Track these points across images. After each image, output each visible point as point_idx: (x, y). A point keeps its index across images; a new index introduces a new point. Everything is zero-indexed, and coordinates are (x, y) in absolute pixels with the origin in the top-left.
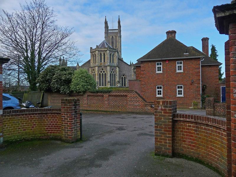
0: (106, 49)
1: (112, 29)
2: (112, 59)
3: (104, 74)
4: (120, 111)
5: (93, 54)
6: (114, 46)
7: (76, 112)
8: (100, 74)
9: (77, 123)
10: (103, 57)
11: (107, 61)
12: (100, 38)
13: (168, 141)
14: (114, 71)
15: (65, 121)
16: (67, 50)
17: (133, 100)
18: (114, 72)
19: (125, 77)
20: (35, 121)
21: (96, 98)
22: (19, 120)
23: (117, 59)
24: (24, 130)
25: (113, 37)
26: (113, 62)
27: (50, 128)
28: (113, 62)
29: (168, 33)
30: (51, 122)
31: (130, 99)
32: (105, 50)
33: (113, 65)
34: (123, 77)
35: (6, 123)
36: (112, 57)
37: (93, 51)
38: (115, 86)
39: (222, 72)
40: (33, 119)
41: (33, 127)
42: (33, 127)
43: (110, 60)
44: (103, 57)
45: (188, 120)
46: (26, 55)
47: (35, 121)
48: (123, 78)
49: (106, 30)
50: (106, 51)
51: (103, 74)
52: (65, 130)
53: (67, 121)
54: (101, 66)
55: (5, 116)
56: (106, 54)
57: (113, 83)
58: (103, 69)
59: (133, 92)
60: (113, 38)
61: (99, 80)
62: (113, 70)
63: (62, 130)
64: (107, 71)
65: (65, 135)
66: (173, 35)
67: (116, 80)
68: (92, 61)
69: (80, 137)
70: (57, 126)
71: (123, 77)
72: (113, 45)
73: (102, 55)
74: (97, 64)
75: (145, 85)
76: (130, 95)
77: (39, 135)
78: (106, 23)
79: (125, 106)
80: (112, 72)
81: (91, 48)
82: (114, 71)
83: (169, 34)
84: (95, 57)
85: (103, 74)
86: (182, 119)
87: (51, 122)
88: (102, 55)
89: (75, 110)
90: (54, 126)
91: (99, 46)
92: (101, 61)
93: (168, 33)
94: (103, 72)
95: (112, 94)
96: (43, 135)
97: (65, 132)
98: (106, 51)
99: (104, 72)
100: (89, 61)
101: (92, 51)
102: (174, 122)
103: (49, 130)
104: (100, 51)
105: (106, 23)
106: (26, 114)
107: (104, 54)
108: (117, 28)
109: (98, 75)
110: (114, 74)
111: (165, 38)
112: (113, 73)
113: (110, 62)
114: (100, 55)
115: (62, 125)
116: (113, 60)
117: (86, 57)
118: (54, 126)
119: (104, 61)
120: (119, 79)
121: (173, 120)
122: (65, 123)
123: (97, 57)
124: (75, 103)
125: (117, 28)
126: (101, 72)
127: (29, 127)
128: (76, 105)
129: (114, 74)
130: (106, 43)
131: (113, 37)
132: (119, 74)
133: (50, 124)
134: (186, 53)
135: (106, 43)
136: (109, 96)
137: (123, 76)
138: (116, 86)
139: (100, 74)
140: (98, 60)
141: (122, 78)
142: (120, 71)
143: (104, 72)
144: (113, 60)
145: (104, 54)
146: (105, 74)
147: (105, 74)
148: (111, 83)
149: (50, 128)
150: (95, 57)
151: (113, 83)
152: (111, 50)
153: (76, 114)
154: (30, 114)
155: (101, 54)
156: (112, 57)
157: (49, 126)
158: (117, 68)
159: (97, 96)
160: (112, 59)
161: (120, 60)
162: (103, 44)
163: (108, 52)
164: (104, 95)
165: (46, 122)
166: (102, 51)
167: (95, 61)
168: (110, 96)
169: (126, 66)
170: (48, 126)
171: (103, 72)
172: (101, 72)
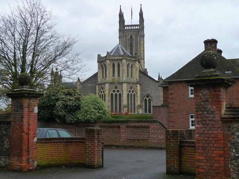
0: (121, 58)
1: (130, 24)
2: (130, 72)
3: (118, 94)
4: (141, 145)
5: (102, 64)
6: (134, 52)
7: (98, 140)
8: (112, 94)
9: (99, 151)
10: (116, 69)
11: (123, 76)
12: (111, 40)
13: (176, 162)
14: (133, 90)
15: (89, 149)
16: (69, 63)
17: (156, 132)
18: (133, 91)
19: (149, 99)
20: (61, 148)
21: (111, 130)
22: (48, 147)
23: (138, 72)
24: (52, 157)
25: (131, 37)
26: (132, 76)
27: (74, 156)
28: (132, 76)
29: (207, 42)
30: (76, 150)
31: (152, 131)
32: (119, 60)
33: (132, 81)
34: (148, 99)
35: (39, 150)
36: (130, 69)
37: (101, 60)
38: (134, 112)
39: (56, 136)
40: (59, 147)
41: (59, 154)
42: (59, 154)
43: (128, 73)
44: (116, 69)
45: (190, 145)
46: (14, 71)
47: (61, 148)
48: (147, 100)
49: (122, 26)
50: (122, 60)
51: (116, 94)
52: (89, 157)
53: (91, 149)
54: (114, 83)
55: (38, 143)
56: (121, 65)
57: (131, 108)
58: (116, 88)
59: (157, 123)
60: (132, 37)
61: (110, 104)
62: (131, 88)
63: (86, 157)
64: (122, 90)
65: (89, 161)
66: (213, 46)
67: (136, 104)
68: (100, 76)
69: (101, 164)
70: (81, 154)
71: (148, 99)
72: (131, 53)
73: (116, 65)
74: (107, 79)
75: (174, 114)
76: (152, 126)
77: (65, 162)
78: (121, 16)
79: (146, 140)
80: (130, 91)
81: (99, 55)
82: (133, 90)
83: (207, 44)
84: (104, 70)
85: (116, 94)
86: (186, 144)
87: (76, 150)
88: (116, 65)
89: (98, 138)
90: (78, 154)
91: (110, 52)
92: (114, 75)
93: (207, 42)
94: (116, 92)
95: (131, 124)
96: (67, 162)
97: (89, 159)
98: (122, 60)
99: (118, 91)
100: (96, 75)
101: (101, 61)
102: (181, 147)
103: (73, 158)
104: (113, 60)
105: (121, 16)
106: (54, 142)
107: (119, 65)
108: (138, 23)
109: (109, 96)
110: (133, 94)
111: (201, 49)
112: (131, 92)
113: (128, 76)
114: (112, 66)
115: (86, 153)
116: (132, 73)
117: (89, 69)
118: (78, 154)
119: (119, 75)
120: (141, 101)
121: (180, 145)
122: (89, 151)
123: (107, 68)
124: (98, 132)
125: (138, 23)
126: (114, 91)
127: (56, 154)
128: (99, 134)
129: (133, 94)
130: (121, 48)
131: (131, 37)
132: (141, 94)
133: (74, 152)
134: (228, 71)
135: (121, 48)
136: (127, 127)
137: (147, 97)
138: (136, 112)
139: (112, 94)
140: (109, 74)
141: (146, 100)
142: (142, 90)
143: (118, 91)
144: (132, 73)
145: (119, 65)
146: (120, 94)
147: (120, 94)
148: (128, 107)
149: (74, 156)
150: (104, 70)
151: (131, 108)
152: (129, 58)
153: (99, 142)
154: (57, 142)
155: (114, 65)
156: (130, 69)
157: (73, 154)
158: (138, 86)
159: (111, 127)
160: (130, 72)
161: (144, 73)
162: (117, 50)
163: (124, 61)
164: (121, 126)
165: (70, 150)
166: (115, 60)
167: (104, 74)
168: (128, 127)
169: (151, 81)
170: (73, 154)
171: (116, 92)
172: (114, 91)
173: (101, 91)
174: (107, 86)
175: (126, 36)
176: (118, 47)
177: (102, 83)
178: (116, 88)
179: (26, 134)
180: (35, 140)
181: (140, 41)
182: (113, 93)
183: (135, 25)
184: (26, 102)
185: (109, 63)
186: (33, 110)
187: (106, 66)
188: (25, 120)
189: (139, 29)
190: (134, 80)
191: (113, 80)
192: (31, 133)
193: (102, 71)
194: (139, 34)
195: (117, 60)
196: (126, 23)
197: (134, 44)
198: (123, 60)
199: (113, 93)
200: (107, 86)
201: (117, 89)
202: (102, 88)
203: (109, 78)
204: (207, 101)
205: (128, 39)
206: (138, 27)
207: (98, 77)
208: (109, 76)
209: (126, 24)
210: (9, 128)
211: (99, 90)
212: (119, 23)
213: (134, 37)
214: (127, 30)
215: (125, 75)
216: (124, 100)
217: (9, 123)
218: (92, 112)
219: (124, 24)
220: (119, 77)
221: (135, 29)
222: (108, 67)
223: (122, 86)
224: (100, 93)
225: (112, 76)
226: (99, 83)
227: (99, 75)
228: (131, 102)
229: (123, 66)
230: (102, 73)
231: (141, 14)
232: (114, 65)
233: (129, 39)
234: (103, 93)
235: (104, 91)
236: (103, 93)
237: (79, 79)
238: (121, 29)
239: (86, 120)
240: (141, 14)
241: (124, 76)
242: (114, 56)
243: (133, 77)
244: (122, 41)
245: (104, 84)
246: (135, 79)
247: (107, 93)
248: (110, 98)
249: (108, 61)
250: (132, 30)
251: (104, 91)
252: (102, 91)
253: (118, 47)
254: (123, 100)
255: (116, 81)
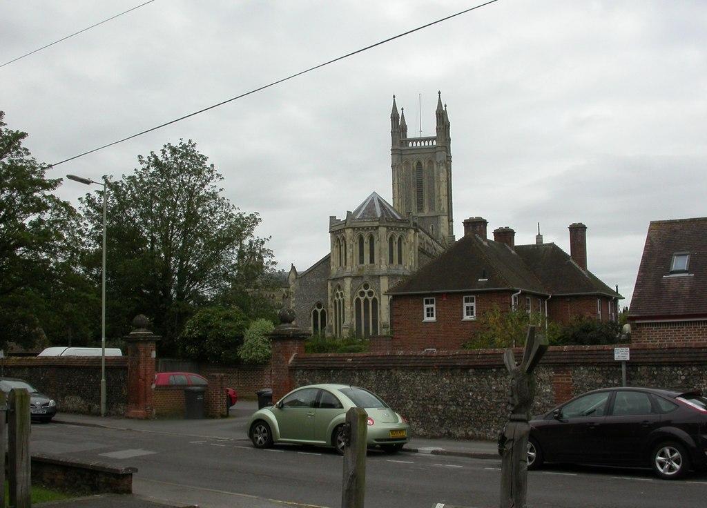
0: (376, 224)
3: (370, 299)
8: (358, 300)
10: (367, 247)
11: (380, 261)
25: (419, 164)
26: (400, 262)
28: (400, 262)
32: (372, 227)
36: (396, 247)
37: (337, 228)
44: (367, 247)
50: (377, 227)
51: (366, 301)
54: (362, 277)
56: (376, 239)
58: (366, 286)
61: (354, 320)
73: (366, 240)
74: (349, 268)
84: (343, 248)
85: (366, 301)
88: (366, 240)
91: (355, 212)
92: (362, 262)
94: (366, 295)
98: (377, 227)
99: (370, 293)
100: (327, 260)
101: (338, 230)
104: (359, 229)
107: (372, 239)
108: (434, 134)
109: (352, 305)
113: (391, 261)
119: (372, 261)
123: (348, 246)
125: (434, 134)
131: (419, 164)
139: (358, 300)
140: (352, 257)
145: (372, 239)
147: (375, 301)
150: (343, 248)
155: (361, 239)
156: (396, 247)
166: (363, 228)
171: (366, 295)
172: (362, 294)
173: (338, 294)
174: (348, 282)
175: (407, 163)
176: (373, 200)
177: (339, 276)
178: (366, 286)
179: (143, 380)
180: (154, 386)
181: (438, 174)
182: (361, 298)
183: (428, 139)
184: (142, 347)
185: (351, 235)
186: (150, 354)
187: (345, 242)
188: (142, 366)
189: (435, 148)
190: (406, 269)
191: (359, 270)
192: (148, 378)
193: (338, 250)
194: (435, 158)
195: (368, 228)
196: (411, 134)
197: (425, 182)
198: (380, 228)
199: (361, 298)
200: (348, 282)
201: (363, 290)
202: (339, 287)
203: (352, 267)
204: (280, 352)
205: (412, 169)
206: (435, 143)
207: (332, 263)
208: (353, 261)
209: (410, 135)
210: (127, 373)
211: (334, 291)
212: (392, 135)
213: (425, 165)
214: (413, 149)
215: (385, 259)
216: (382, 312)
217: (126, 368)
218: (259, 346)
219: (406, 137)
220: (374, 263)
221: (429, 148)
222: (349, 242)
223: (379, 282)
224: (336, 298)
225: (358, 261)
226: (334, 277)
227: (332, 260)
228: (340, 315)
229: (380, 241)
230: (339, 256)
231: (442, 116)
232: (361, 239)
233: (413, 170)
234: (340, 297)
235: (342, 294)
236: (340, 297)
237: (293, 268)
238: (396, 147)
239: (251, 360)
240: (442, 116)
241: (383, 262)
242: (362, 219)
243: (403, 264)
244: (398, 175)
245: (342, 278)
246: (407, 268)
247: (348, 297)
248: (354, 310)
249: (348, 232)
250: (421, 148)
251: (342, 294)
252: (339, 293)
253: (373, 200)
254: (380, 311)
255: (366, 272)
